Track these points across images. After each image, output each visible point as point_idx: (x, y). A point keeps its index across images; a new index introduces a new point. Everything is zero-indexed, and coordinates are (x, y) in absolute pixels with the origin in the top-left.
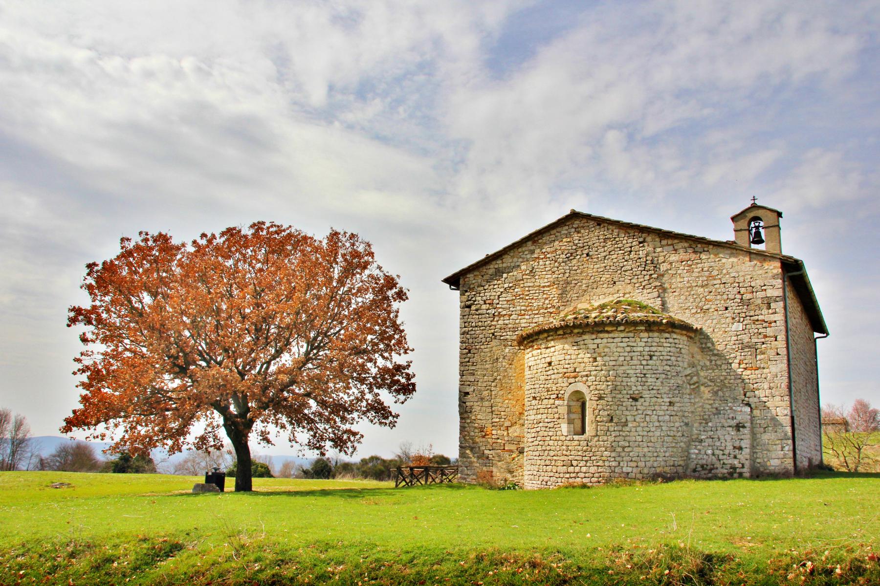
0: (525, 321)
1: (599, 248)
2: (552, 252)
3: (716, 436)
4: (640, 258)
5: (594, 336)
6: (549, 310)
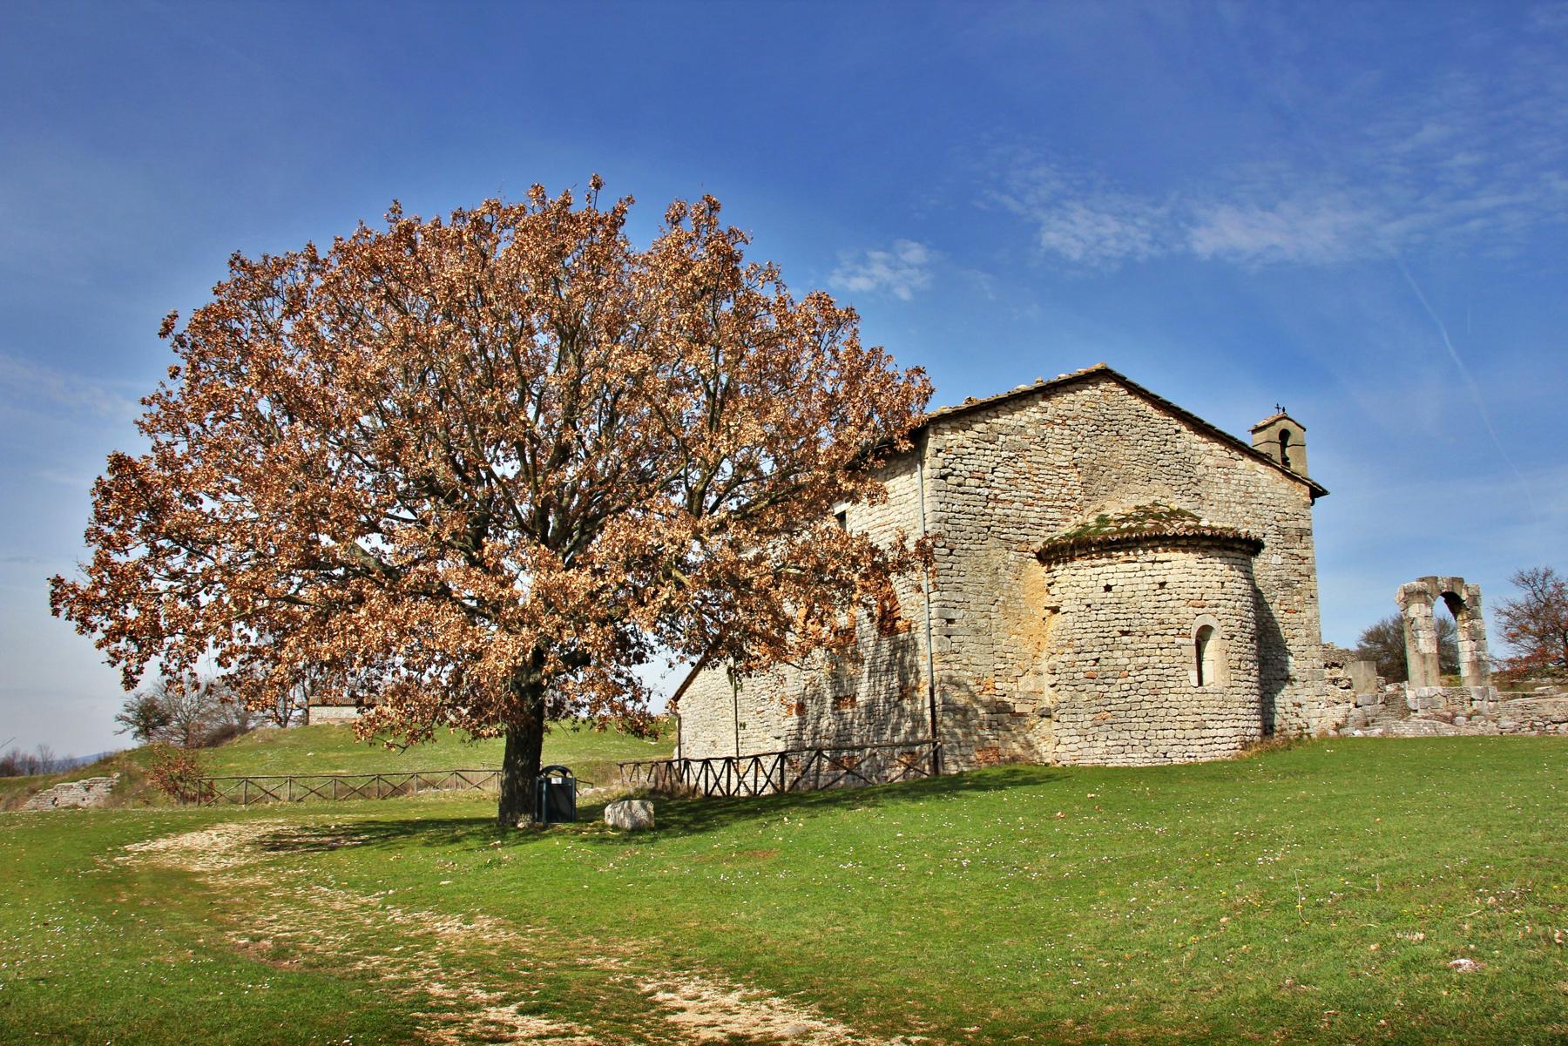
0: (1035, 515)
2: (1073, 419)
6: (1068, 503)
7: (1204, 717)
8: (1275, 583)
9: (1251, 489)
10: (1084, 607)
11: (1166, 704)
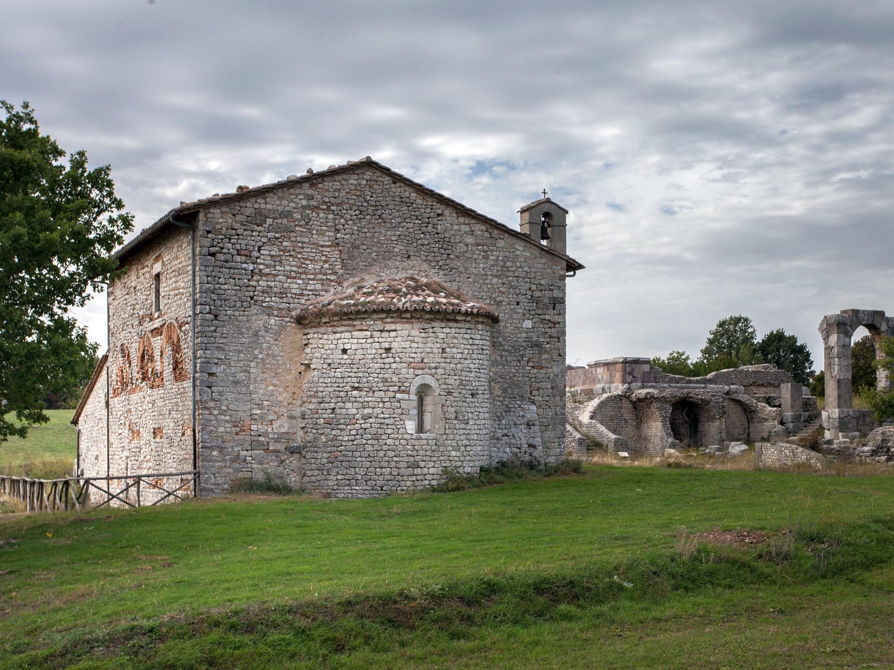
1: (393, 211)
2: (337, 205)
3: (511, 434)
4: (438, 234)
5: (444, 325)
6: (329, 277)
7: (418, 458)
9: (509, 264)
10: (326, 366)
11: (385, 448)
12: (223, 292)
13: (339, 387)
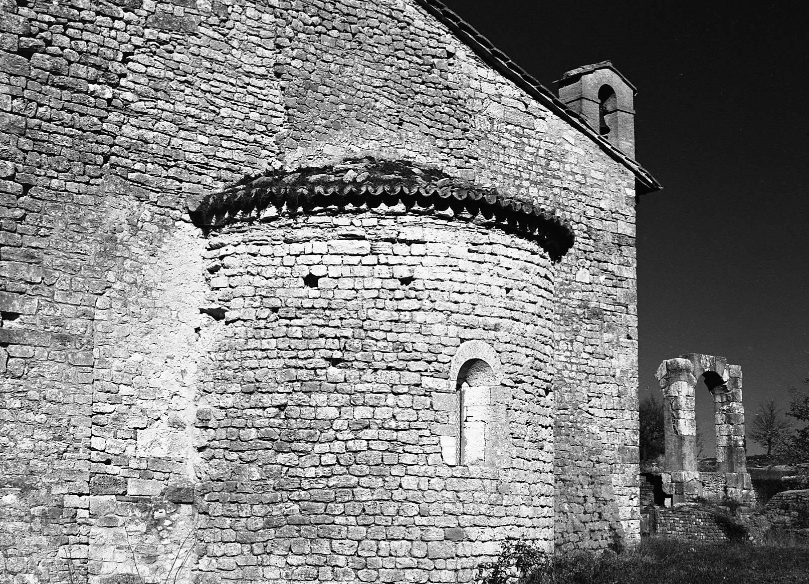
0: (198, 148)
4: (448, 88)
6: (258, 138)
7: (465, 520)
8: (579, 311)
10: (266, 313)
11: (398, 495)
12: (45, 136)
13: (296, 357)
